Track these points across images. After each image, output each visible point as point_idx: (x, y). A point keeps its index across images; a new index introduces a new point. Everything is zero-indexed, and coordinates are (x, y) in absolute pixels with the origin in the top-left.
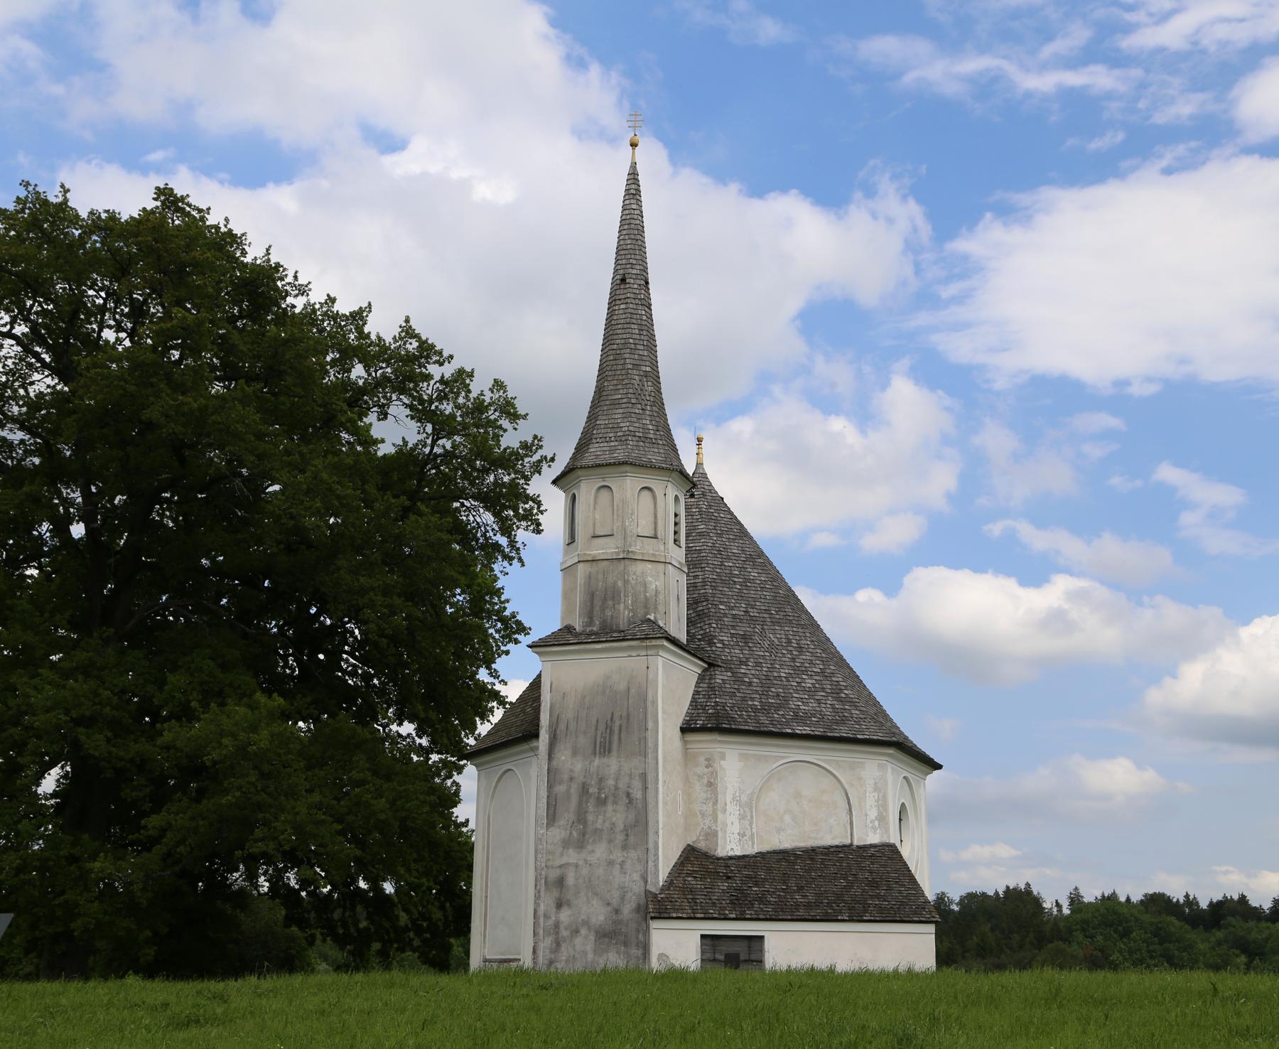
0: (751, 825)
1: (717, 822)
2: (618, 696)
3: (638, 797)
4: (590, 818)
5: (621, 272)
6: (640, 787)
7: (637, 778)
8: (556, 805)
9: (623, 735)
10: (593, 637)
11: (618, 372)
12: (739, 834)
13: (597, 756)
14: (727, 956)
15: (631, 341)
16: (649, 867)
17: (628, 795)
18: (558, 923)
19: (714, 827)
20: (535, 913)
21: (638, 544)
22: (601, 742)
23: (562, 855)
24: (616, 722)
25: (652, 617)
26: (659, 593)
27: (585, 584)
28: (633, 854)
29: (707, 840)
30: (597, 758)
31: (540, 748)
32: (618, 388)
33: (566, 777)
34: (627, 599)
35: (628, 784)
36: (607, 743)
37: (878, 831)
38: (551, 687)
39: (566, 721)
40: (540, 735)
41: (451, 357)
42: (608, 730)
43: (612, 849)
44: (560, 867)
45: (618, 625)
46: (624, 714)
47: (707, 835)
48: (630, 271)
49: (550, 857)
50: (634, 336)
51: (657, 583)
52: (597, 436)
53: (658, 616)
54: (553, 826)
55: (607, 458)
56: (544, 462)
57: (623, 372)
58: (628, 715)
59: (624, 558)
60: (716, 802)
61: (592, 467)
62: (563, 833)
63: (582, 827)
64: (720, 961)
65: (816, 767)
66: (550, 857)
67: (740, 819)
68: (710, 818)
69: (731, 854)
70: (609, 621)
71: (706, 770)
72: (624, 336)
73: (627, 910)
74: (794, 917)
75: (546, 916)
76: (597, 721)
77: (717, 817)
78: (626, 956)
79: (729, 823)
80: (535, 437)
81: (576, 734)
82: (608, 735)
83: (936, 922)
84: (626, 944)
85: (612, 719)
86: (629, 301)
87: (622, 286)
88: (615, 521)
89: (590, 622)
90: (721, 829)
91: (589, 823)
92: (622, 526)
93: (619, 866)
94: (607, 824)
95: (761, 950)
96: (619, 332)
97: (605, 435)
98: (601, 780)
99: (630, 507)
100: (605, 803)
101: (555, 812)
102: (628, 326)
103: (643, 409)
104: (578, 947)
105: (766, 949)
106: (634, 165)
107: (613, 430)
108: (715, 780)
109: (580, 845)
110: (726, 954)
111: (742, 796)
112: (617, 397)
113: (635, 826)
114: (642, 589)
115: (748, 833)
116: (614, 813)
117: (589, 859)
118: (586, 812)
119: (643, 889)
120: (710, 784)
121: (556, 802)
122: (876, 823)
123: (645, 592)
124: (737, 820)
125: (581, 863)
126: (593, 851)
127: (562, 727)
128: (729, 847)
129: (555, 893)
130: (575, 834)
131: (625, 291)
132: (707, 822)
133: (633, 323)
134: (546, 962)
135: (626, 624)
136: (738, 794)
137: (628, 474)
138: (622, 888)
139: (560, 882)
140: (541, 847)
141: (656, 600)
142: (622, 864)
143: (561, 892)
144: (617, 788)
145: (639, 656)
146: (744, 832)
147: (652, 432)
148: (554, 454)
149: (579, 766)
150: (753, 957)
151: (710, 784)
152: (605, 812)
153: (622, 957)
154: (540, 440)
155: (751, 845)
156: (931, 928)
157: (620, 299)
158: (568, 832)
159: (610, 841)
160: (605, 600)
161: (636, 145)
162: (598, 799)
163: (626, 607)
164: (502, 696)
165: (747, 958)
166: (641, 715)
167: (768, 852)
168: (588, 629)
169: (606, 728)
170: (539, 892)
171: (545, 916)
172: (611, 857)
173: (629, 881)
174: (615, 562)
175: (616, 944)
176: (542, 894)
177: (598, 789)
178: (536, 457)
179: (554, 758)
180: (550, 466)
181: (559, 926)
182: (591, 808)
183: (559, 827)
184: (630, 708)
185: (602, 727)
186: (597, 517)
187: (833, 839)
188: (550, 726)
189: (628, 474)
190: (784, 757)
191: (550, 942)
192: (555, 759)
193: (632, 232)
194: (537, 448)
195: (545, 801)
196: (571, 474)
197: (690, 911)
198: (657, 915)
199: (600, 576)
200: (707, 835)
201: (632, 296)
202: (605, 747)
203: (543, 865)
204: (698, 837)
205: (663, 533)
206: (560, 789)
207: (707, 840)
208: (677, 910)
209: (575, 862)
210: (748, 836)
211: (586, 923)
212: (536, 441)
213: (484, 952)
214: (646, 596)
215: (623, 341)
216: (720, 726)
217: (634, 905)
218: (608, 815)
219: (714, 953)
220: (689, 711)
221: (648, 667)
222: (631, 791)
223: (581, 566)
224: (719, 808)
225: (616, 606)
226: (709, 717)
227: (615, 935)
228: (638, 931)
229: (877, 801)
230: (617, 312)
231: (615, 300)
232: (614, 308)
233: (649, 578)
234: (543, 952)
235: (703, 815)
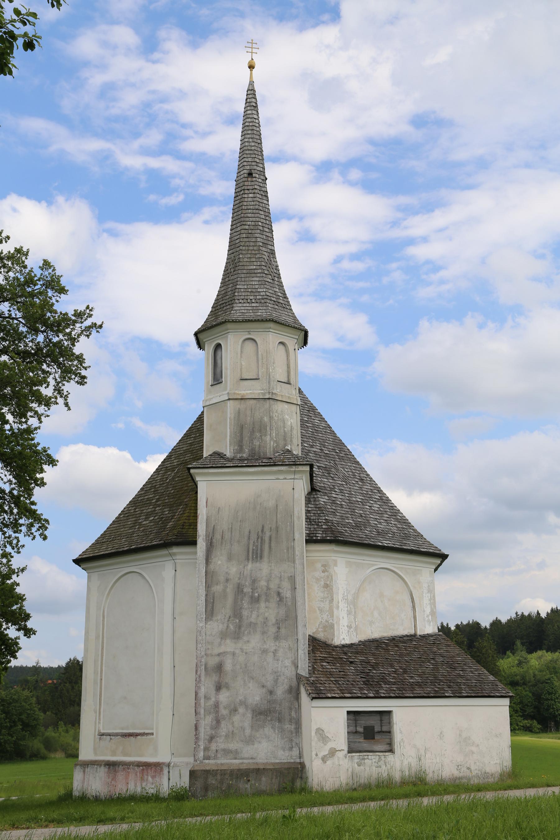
0: (355, 619)
1: (333, 617)
2: (268, 512)
3: (287, 596)
4: (245, 613)
5: (248, 167)
6: (289, 587)
7: (286, 580)
8: (213, 602)
9: (273, 544)
10: (246, 462)
11: (251, 248)
12: (347, 626)
13: (250, 561)
14: (365, 728)
15: (260, 224)
16: (299, 655)
17: (279, 594)
18: (218, 703)
19: (331, 621)
20: (196, 695)
21: (278, 388)
22: (253, 550)
23: (220, 645)
24: (267, 532)
25: (289, 448)
26: (293, 428)
27: (234, 418)
28: (284, 644)
29: (325, 631)
30: (250, 562)
31: (198, 554)
32: (252, 260)
33: (222, 578)
34: (272, 432)
35: (278, 585)
36: (259, 550)
37: (431, 624)
38: (207, 502)
39: (221, 531)
40: (198, 542)
41: (8, 237)
42: (260, 540)
43: (265, 639)
44: (219, 655)
45: (265, 453)
46: (274, 526)
47: (325, 627)
48: (255, 167)
49: (210, 647)
50: (262, 220)
51: (292, 421)
52: (239, 298)
53: (293, 448)
54: (211, 620)
55: (250, 315)
56: (94, 328)
57: (255, 248)
58: (277, 528)
59: (269, 399)
60: (332, 600)
61: (243, 321)
62: (221, 626)
63: (237, 621)
64: (360, 733)
65: (392, 573)
66: (210, 647)
67: (348, 615)
68: (327, 613)
69: (343, 642)
70: (257, 449)
71: (323, 574)
72: (254, 219)
73: (280, 692)
74: (416, 695)
75: (207, 698)
76: (250, 532)
77: (333, 612)
78: (280, 730)
79: (341, 618)
80: (88, 307)
81: (231, 542)
82: (259, 544)
83: (510, 697)
84: (280, 720)
85: (262, 531)
86: (256, 191)
87: (250, 179)
88: (260, 368)
89: (241, 449)
90: (336, 622)
91: (245, 618)
92: (267, 372)
93: (271, 654)
94: (261, 619)
95: (390, 723)
96: (249, 215)
97: (246, 297)
98: (254, 581)
99: (272, 357)
100: (258, 601)
101: (213, 608)
102: (257, 211)
103: (273, 280)
104: (236, 724)
105: (394, 722)
106: (251, 83)
107: (252, 294)
108: (330, 582)
109: (237, 636)
110: (364, 727)
111: (349, 595)
112: (252, 267)
113: (286, 620)
114: (282, 425)
115: (353, 626)
116: (267, 610)
117: (245, 648)
118: (241, 608)
119: (294, 673)
120: (326, 586)
121: (214, 600)
122: (430, 617)
123: (284, 427)
124: (346, 615)
125: (237, 651)
126: (248, 641)
127: (218, 536)
128: (341, 637)
129: (215, 678)
130: (231, 627)
131: (253, 183)
132: (325, 617)
133: (261, 210)
134: (208, 737)
135: (272, 453)
136: (346, 594)
137: (271, 330)
138: (276, 673)
139: (219, 668)
140: (200, 638)
141: (291, 434)
142: (275, 652)
143: (220, 677)
144: (268, 588)
145: (285, 479)
146: (351, 625)
147: (281, 298)
148: (103, 322)
149: (234, 570)
150: (385, 729)
151: (326, 586)
152: (258, 608)
153: (277, 731)
154: (91, 310)
155: (355, 636)
156: (507, 701)
157: (248, 190)
158: (225, 625)
159: (264, 633)
160: (253, 432)
161: (253, 68)
162: (252, 597)
163: (271, 439)
164: (38, 515)
165: (380, 730)
166: (289, 528)
167: (366, 641)
168: (239, 456)
169: (258, 538)
170: (200, 677)
171: (205, 697)
172: (265, 646)
173: (282, 667)
174: (262, 401)
175: (271, 720)
176: (203, 678)
177: (252, 589)
178: (88, 323)
179: (211, 562)
180: (97, 331)
181: (218, 706)
182: (245, 605)
183: (217, 620)
184: (278, 522)
185: (254, 537)
186: (243, 363)
187: (404, 630)
188: (207, 535)
189: (271, 330)
190: (373, 565)
191: (210, 720)
192: (213, 564)
193: (255, 136)
194: (87, 317)
195: (203, 598)
196: (218, 327)
197: (339, 692)
198: (317, 696)
199: (249, 413)
200: (325, 627)
201: (258, 187)
202: (257, 554)
203: (203, 653)
204: (317, 629)
205: (294, 381)
206: (217, 589)
207: (325, 631)
208: (331, 691)
209: (232, 650)
210: (353, 628)
211: (243, 703)
212: (88, 310)
213: (99, 727)
214: (284, 431)
215: (253, 223)
216: (337, 538)
217: (286, 687)
218: (262, 611)
219: (356, 726)
220: (307, 526)
221: (293, 489)
222: (281, 591)
223: (230, 404)
224: (335, 606)
225: (263, 437)
226: (325, 531)
227: (270, 713)
228: (291, 709)
229: (430, 600)
230: (246, 200)
231: (244, 190)
232: (244, 196)
233: (287, 416)
234: (204, 729)
235: (321, 611)
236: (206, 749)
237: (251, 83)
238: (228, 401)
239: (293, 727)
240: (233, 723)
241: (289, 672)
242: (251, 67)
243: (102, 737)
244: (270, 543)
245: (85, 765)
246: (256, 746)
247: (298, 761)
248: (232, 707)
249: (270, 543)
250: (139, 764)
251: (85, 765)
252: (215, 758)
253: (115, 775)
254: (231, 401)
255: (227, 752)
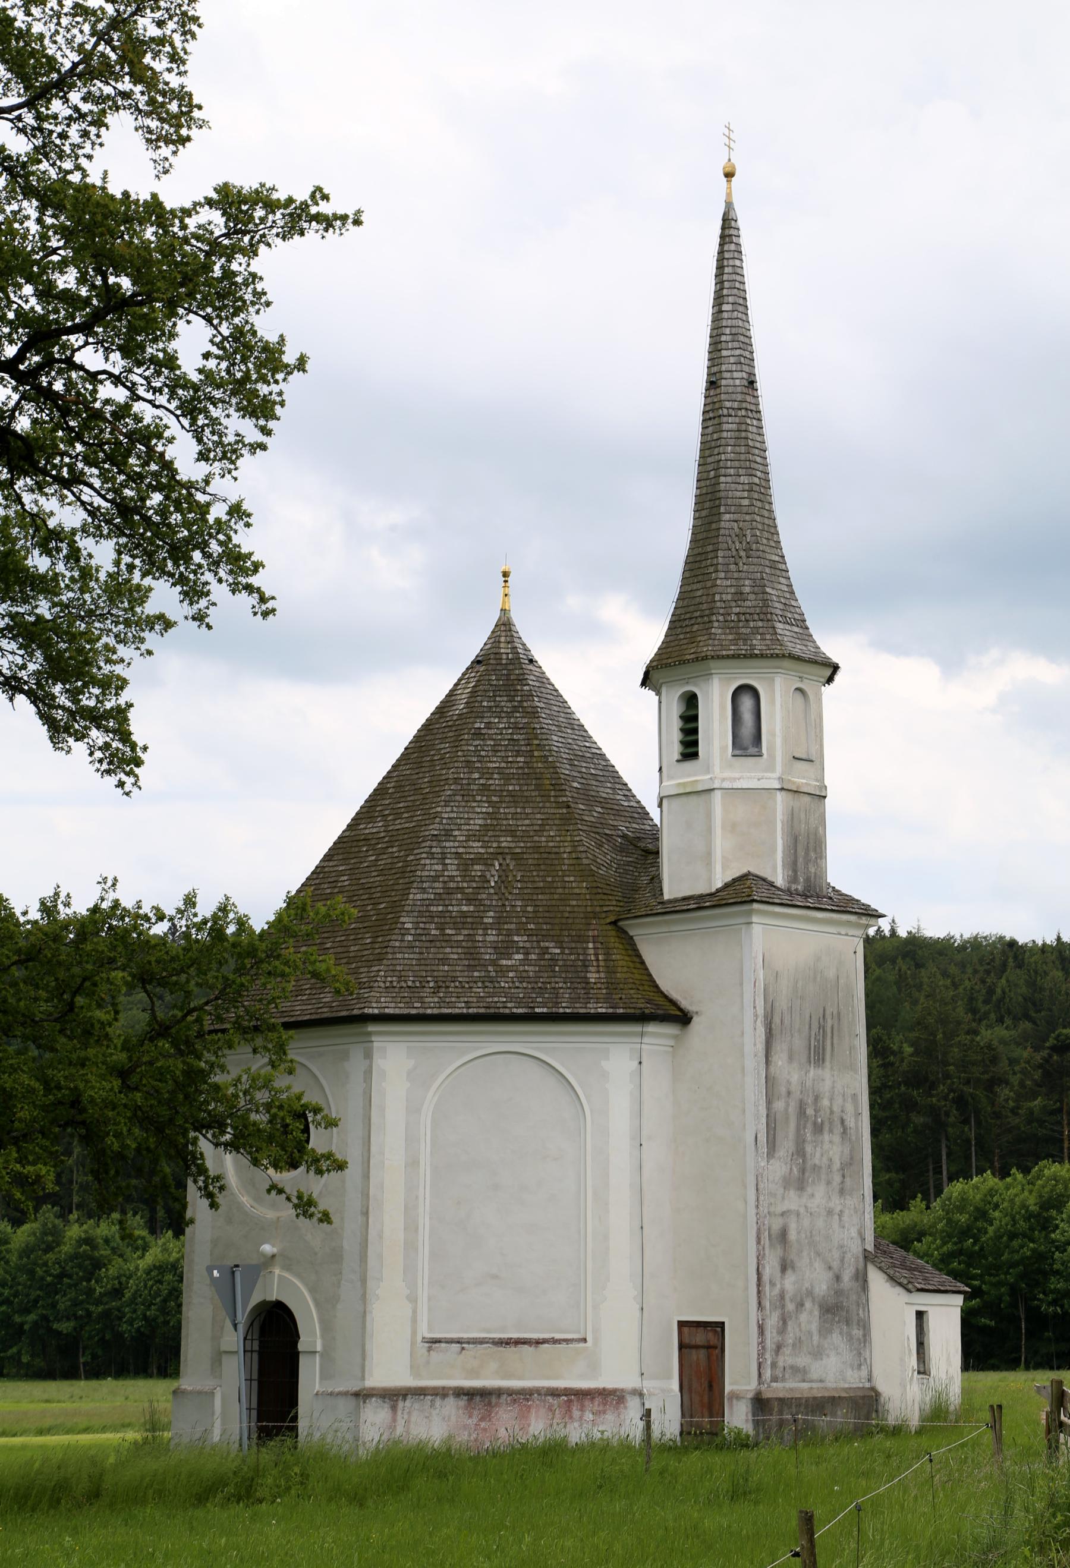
4: (809, 1149)
33: (783, 1090)
44: (783, 1214)
46: (835, 1013)
54: (773, 1157)
58: (839, 1014)
66: (772, 1201)
73: (847, 1276)
91: (808, 1156)
93: (836, 1217)
98: (817, 1098)
106: (729, 206)
125: (802, 1210)
127: (777, 1020)
142: (841, 1214)
143: (785, 1250)
159: (829, 1183)
162: (815, 1123)
171: (770, 1282)
175: (839, 1322)
176: (767, 1251)
195: (764, 1120)
206: (779, 1105)
211: (810, 1293)
218: (826, 1146)
222: (845, 1117)
236: (774, 1365)
237: (729, 206)
238: (778, 792)
239: (861, 1333)
240: (800, 1325)
241: (855, 1249)
242: (729, 175)
243: (434, 1346)
244: (832, 1037)
245: (395, 1395)
246: (824, 1362)
247: (867, 1385)
248: (799, 1299)
249: (832, 1037)
250: (554, 1393)
251: (395, 1395)
252: (783, 1380)
253: (490, 1412)
254: (783, 793)
255: (795, 1369)
